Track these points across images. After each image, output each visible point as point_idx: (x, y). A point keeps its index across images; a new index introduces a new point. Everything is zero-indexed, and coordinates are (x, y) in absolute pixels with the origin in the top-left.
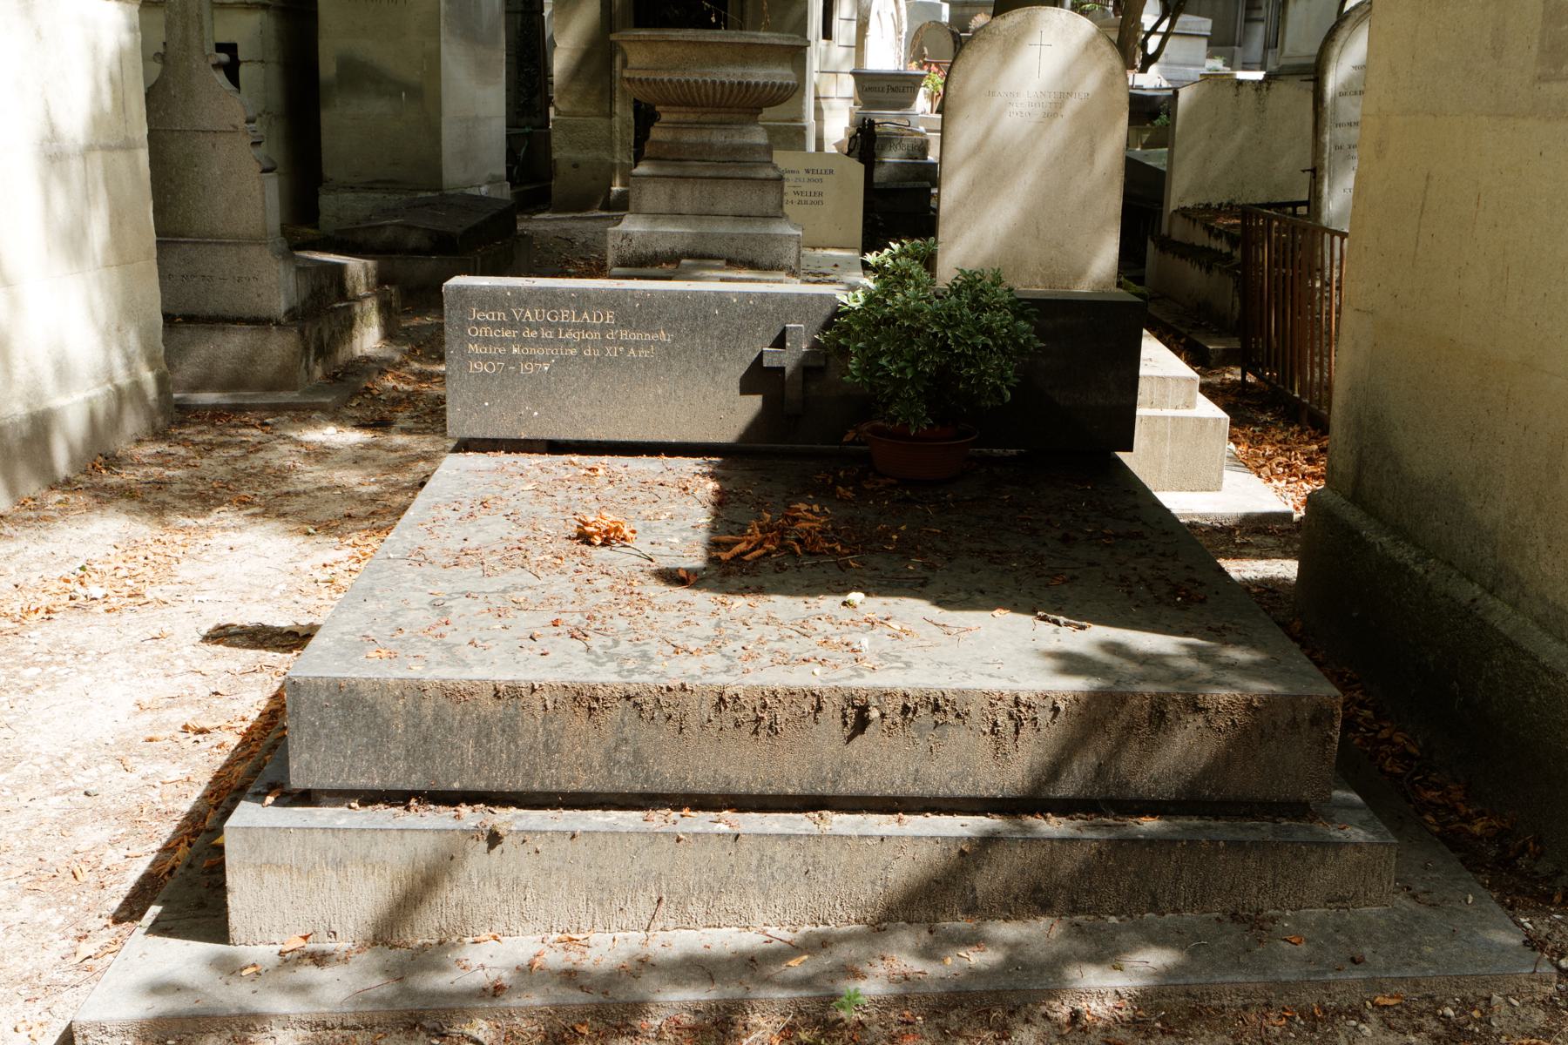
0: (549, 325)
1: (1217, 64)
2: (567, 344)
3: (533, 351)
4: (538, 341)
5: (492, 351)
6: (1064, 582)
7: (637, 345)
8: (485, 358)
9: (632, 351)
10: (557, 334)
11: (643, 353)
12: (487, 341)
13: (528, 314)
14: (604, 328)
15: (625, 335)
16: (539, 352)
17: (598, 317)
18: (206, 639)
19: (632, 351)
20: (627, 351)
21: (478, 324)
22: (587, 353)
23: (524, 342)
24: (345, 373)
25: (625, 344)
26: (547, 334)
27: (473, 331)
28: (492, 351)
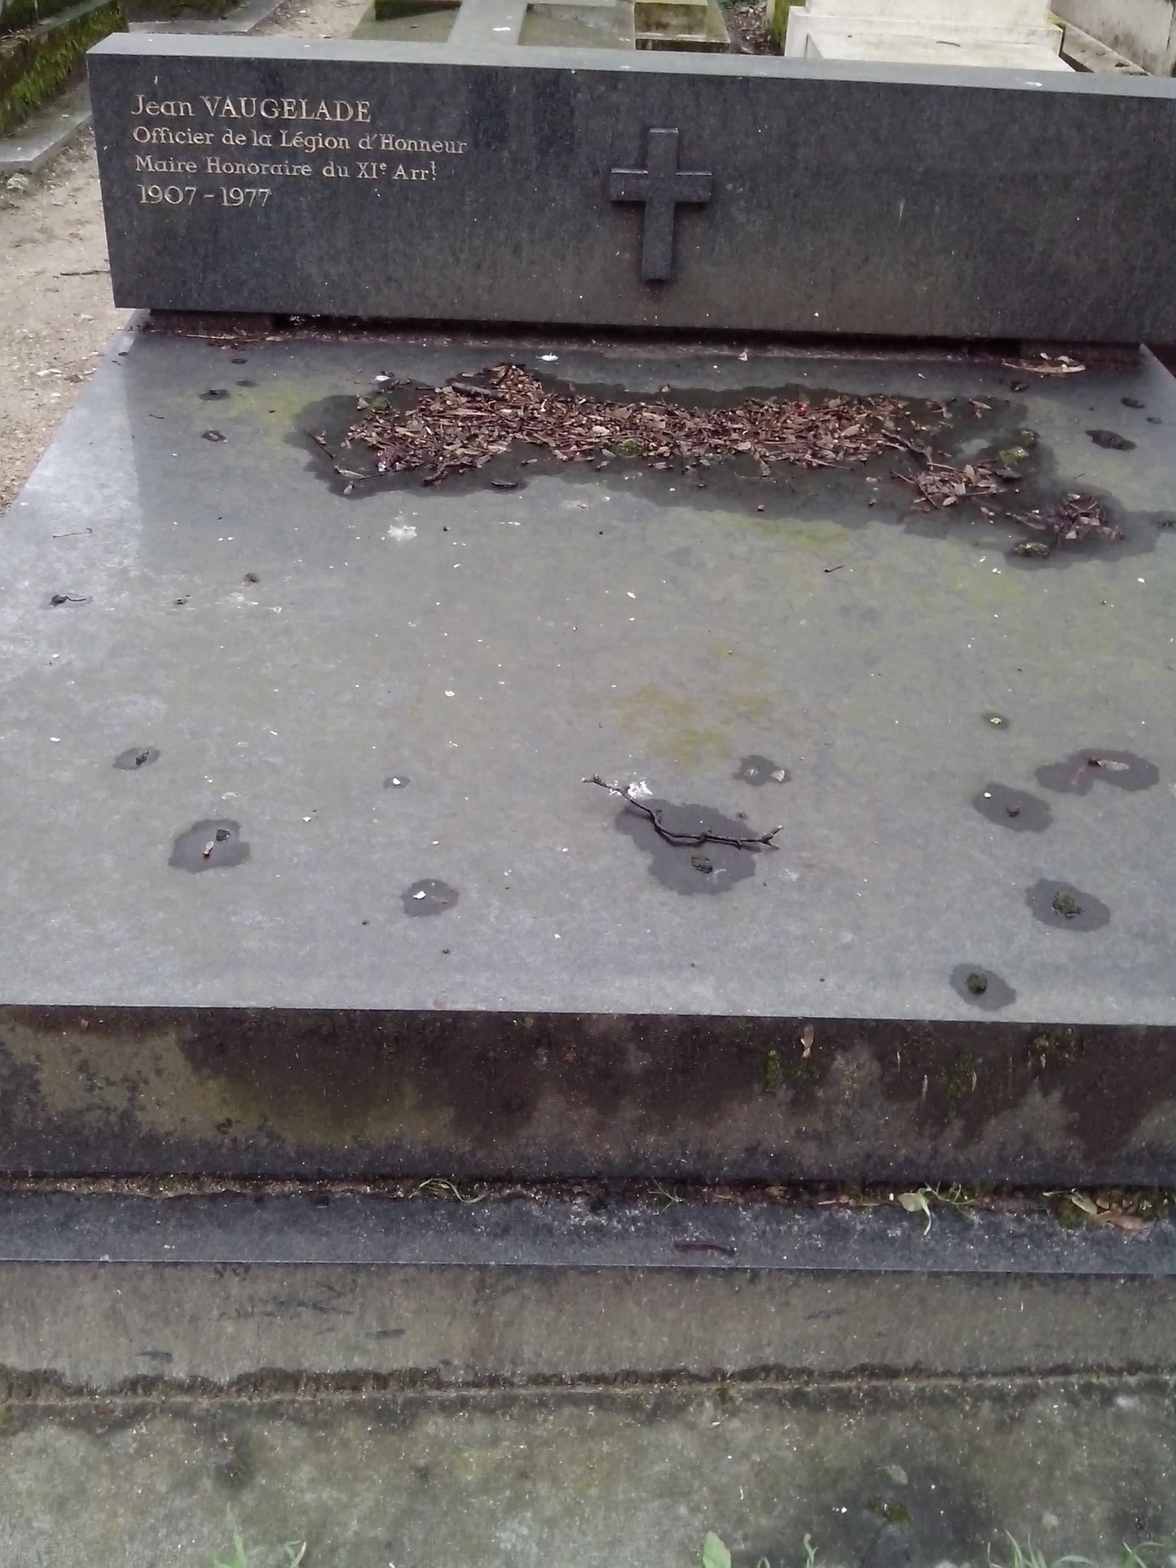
0: (264, 126)
1: (949, 1485)
2: (294, 155)
3: (240, 168)
4: (245, 152)
5: (176, 167)
6: (92, 1393)
7: (411, 160)
8: (163, 180)
9: (401, 170)
10: (277, 139)
11: (901, 448)
12: (162, 152)
13: (229, 106)
14: (352, 130)
15: (387, 142)
16: (254, 169)
17: (344, 112)
18: (1142, 407)
19: (401, 170)
20: (392, 169)
21: (150, 122)
22: (328, 172)
23: (218, 148)
24: (1164, 525)
25: (392, 158)
26: (261, 140)
27: (142, 135)
28: (176, 167)
